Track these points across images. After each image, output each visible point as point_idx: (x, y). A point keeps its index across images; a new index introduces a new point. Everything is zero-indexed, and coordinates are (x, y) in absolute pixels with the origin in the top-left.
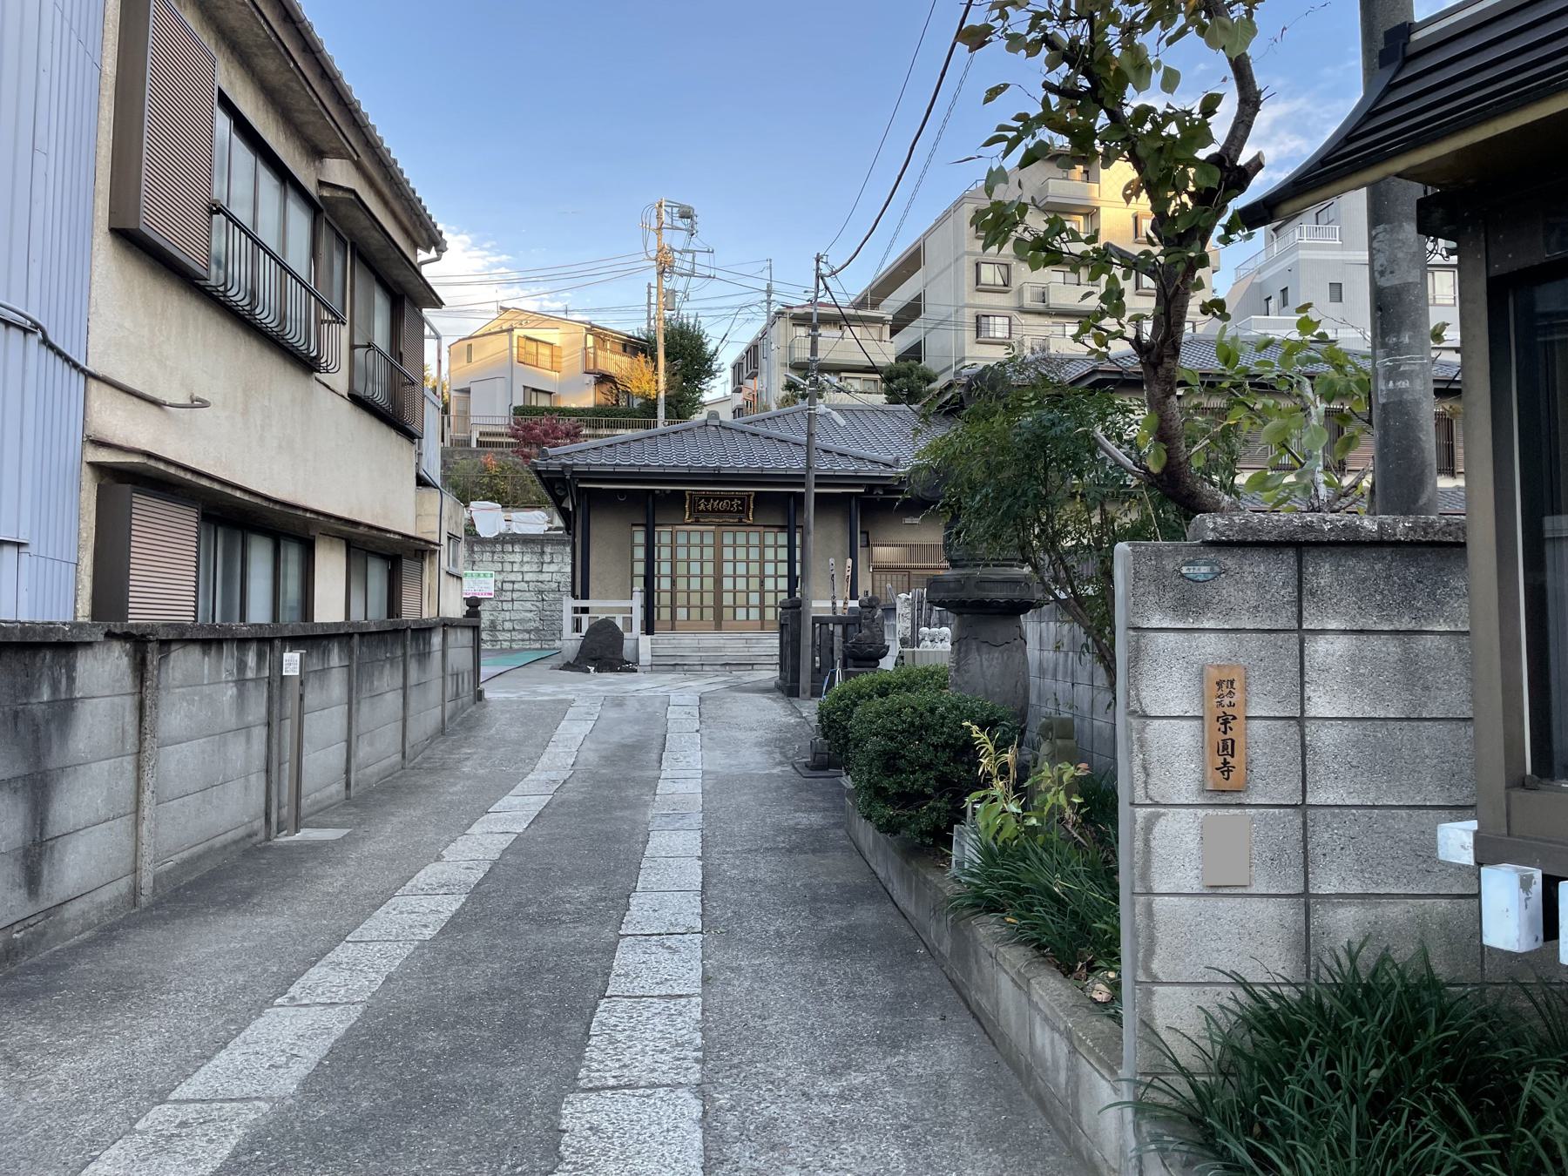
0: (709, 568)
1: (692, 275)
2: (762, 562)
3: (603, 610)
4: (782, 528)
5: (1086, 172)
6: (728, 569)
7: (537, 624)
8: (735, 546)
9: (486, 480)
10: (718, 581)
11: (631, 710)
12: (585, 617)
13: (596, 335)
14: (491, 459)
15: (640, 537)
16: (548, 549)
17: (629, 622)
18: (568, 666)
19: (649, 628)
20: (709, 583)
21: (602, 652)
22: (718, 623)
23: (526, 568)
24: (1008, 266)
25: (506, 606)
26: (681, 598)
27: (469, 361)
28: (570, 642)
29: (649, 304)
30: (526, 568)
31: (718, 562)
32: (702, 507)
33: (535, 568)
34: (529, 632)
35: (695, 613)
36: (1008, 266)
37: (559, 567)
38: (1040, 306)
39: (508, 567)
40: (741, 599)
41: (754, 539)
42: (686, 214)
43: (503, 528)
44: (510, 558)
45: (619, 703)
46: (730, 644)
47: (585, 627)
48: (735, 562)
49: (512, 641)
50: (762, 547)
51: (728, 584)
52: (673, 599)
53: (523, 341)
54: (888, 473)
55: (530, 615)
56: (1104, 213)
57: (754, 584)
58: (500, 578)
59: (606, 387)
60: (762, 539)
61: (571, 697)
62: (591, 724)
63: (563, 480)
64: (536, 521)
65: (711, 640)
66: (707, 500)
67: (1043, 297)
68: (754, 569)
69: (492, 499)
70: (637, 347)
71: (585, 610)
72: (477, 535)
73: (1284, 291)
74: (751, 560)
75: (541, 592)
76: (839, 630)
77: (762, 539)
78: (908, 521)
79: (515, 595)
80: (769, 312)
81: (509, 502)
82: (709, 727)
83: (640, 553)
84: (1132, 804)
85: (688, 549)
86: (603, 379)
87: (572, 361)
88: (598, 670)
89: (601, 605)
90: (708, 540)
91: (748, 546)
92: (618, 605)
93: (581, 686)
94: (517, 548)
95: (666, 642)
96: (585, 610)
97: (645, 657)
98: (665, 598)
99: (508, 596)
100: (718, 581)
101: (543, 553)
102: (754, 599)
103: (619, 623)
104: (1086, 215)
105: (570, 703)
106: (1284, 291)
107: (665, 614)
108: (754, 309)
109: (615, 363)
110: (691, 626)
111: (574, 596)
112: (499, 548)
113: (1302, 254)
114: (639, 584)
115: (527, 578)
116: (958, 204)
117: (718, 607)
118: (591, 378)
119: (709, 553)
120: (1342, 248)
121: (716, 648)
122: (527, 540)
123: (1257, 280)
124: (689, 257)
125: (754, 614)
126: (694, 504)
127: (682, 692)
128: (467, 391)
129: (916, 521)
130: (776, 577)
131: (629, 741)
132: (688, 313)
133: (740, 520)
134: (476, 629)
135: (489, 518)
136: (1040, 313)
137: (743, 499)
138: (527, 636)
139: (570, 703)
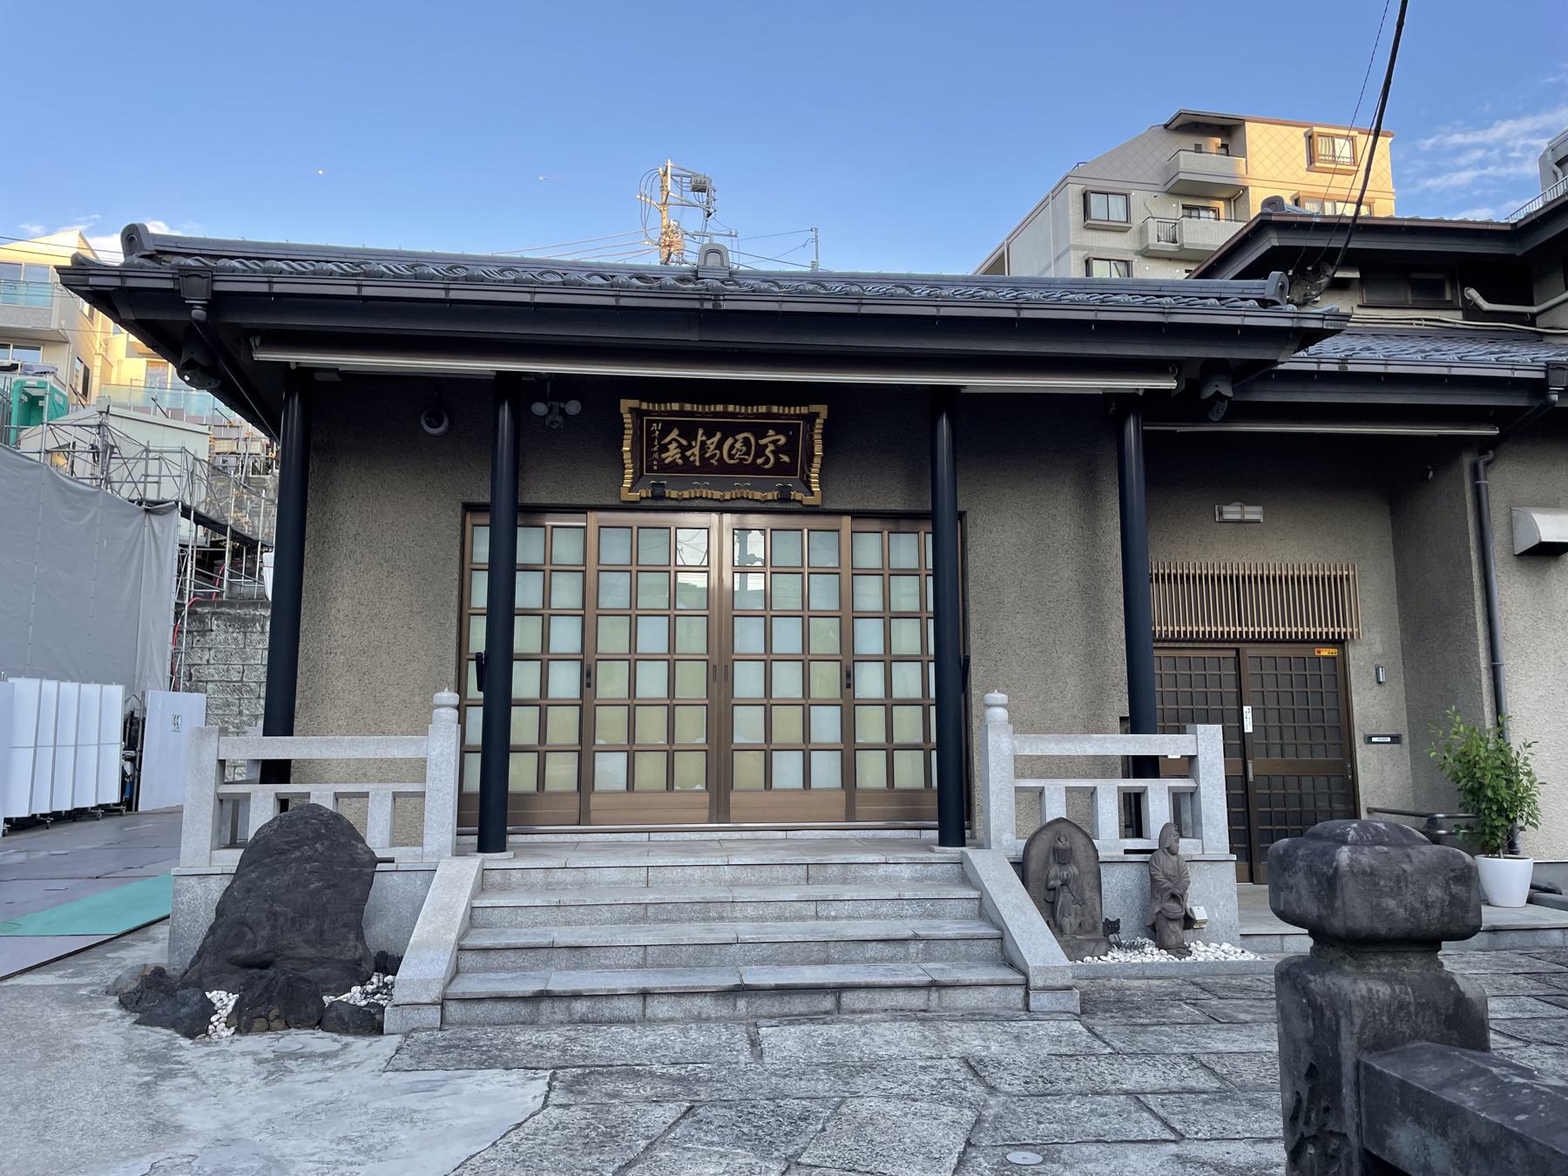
2: (848, 616)
4: (896, 520)
5: (1224, 146)
10: (720, 673)
17: (409, 808)
20: (692, 681)
22: (720, 799)
26: (610, 724)
32: (672, 454)
35: (651, 770)
40: (787, 724)
41: (824, 552)
48: (768, 660)
51: (748, 681)
52: (586, 727)
57: (826, 679)
66: (688, 432)
78: (1232, 512)
84: (584, 572)
92: (393, 761)
102: (826, 724)
104: (1228, 200)
116: (1063, 183)
125: (826, 770)
126: (648, 447)
129: (1254, 513)
130: (889, 659)
133: (785, 498)
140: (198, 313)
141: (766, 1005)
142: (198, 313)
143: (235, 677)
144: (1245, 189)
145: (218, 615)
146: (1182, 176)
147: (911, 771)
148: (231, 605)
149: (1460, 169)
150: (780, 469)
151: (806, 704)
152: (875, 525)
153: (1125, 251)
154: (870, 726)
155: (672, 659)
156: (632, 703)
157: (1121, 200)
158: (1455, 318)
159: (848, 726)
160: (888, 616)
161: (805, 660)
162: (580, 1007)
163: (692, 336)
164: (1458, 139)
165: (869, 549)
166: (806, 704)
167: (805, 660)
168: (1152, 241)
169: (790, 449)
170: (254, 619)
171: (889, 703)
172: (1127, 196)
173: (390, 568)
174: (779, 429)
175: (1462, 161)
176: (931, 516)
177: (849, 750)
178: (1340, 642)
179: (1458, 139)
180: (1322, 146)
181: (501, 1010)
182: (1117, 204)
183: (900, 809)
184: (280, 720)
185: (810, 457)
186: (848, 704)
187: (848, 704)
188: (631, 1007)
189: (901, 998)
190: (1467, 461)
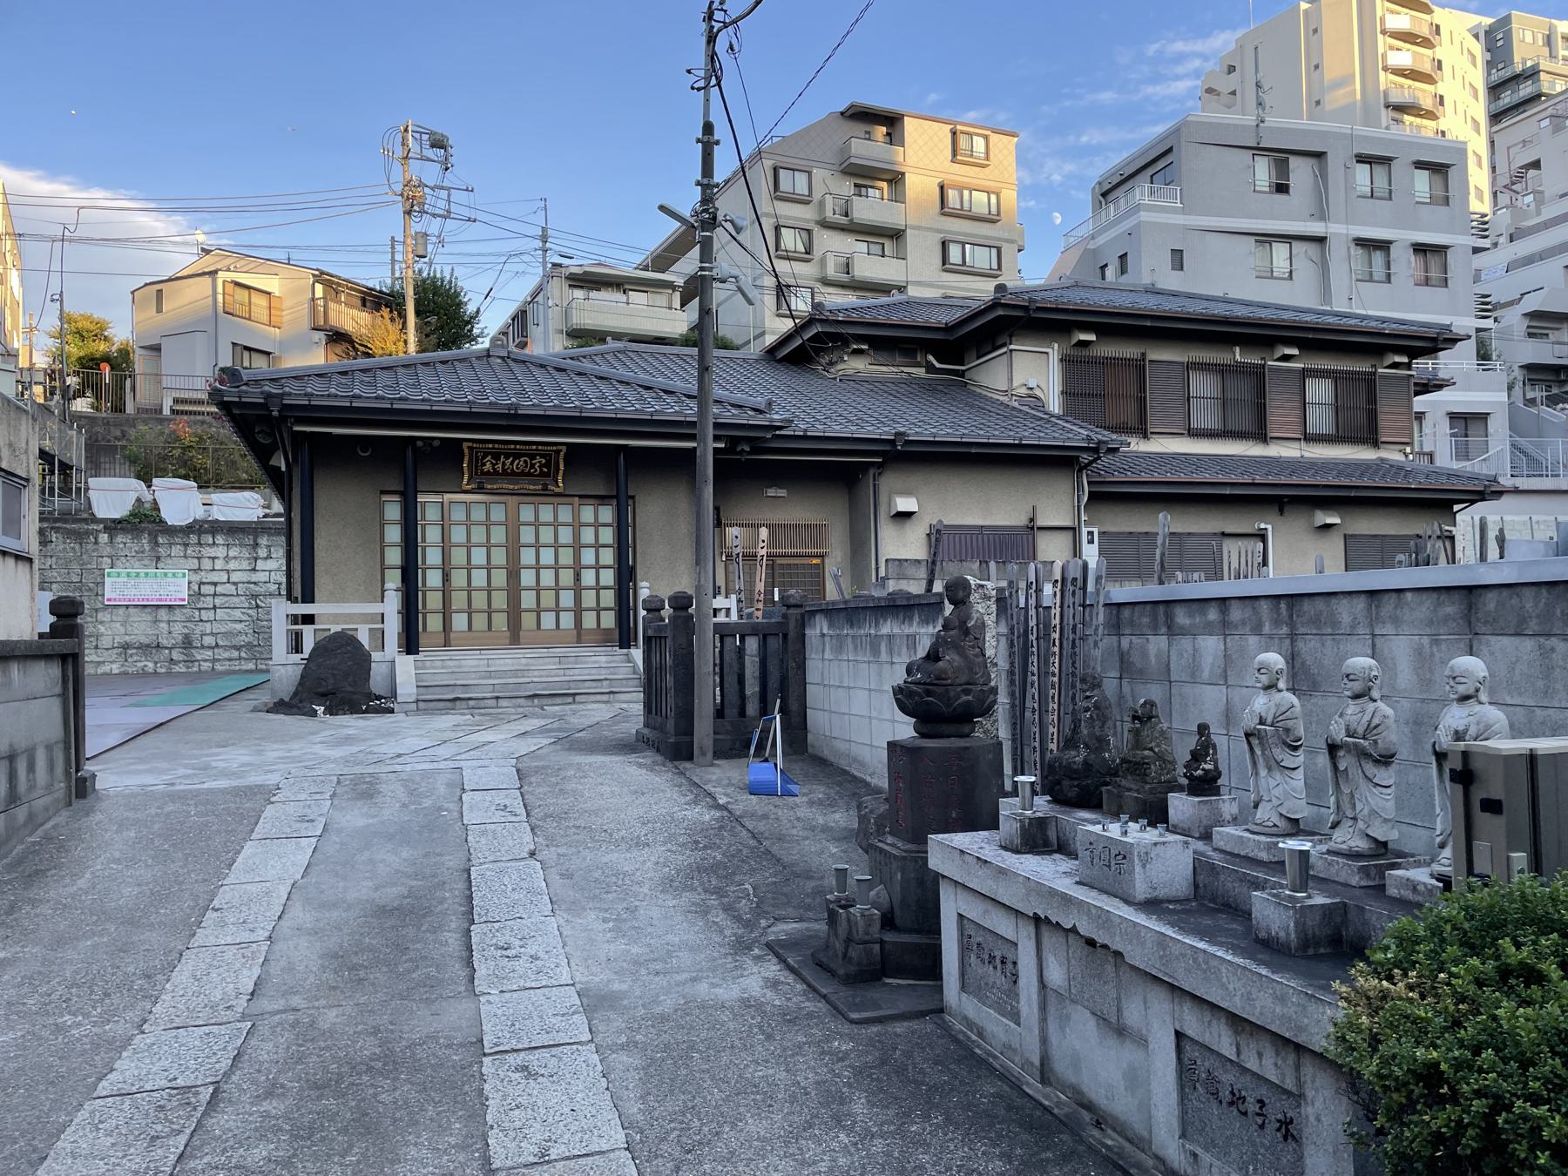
0: (499, 557)
1: (447, 216)
2: (577, 546)
3: (336, 618)
4: (602, 499)
5: (888, 134)
6: (527, 557)
7: (249, 639)
8: (537, 524)
9: (177, 453)
10: (514, 574)
11: (391, 806)
12: (308, 630)
13: (328, 284)
14: (185, 430)
15: (393, 511)
16: (263, 541)
17: (379, 637)
18: (281, 707)
19: (410, 644)
20: (500, 578)
21: (337, 682)
22: (515, 636)
23: (232, 565)
24: (809, 232)
25: (205, 615)
26: (459, 600)
27: (159, 310)
28: (286, 667)
29: (393, 261)
30: (232, 565)
31: (513, 548)
32: (488, 467)
33: (245, 565)
34: (238, 648)
35: (480, 621)
36: (809, 232)
37: (273, 566)
38: (844, 278)
39: (207, 564)
40: (548, 599)
41: (565, 514)
42: (439, 143)
43: (199, 513)
44: (212, 552)
45: (364, 789)
46: (536, 665)
47: (308, 644)
49: (214, 660)
50: (577, 526)
51: (527, 578)
52: (446, 601)
53: (230, 287)
54: (760, 420)
55: (239, 627)
56: (910, 179)
57: (567, 577)
58: (196, 578)
59: (339, 349)
60: (576, 515)
61: (273, 779)
62: (308, 845)
63: (268, 418)
64: (247, 505)
65: (507, 660)
66: (496, 457)
67: (847, 268)
68: (566, 557)
69: (186, 477)
70: (379, 301)
71: (309, 619)
72: (162, 521)
73: (1123, 257)
74: (564, 540)
75: (255, 596)
76: (752, 644)
77: (576, 515)
78: (771, 492)
79: (218, 601)
80: (544, 263)
81: (206, 481)
82: (551, 841)
83: (394, 534)
85: (464, 527)
86: (337, 337)
87: (295, 315)
88: (330, 711)
89: (335, 611)
90: (498, 513)
91: (556, 525)
92: (360, 609)
93: (297, 748)
94: (220, 540)
95: (437, 664)
96: (309, 619)
97: (407, 687)
98: (434, 601)
99: (209, 602)
100: (514, 574)
101: (256, 545)
102: (567, 599)
103: (363, 637)
104: (890, 181)
105: (266, 794)
106: (1123, 257)
107: (434, 623)
108: (526, 258)
109: (352, 319)
110: (473, 640)
111: (290, 597)
112: (193, 539)
113: (1144, 216)
114: (394, 580)
115: (235, 577)
117: (514, 612)
118: (320, 337)
119: (499, 535)
120: (1183, 211)
121: (516, 673)
122: (234, 530)
123: (1091, 246)
124: (444, 194)
125: (567, 620)
126: (476, 464)
127: (488, 754)
128: (157, 349)
129: (782, 493)
130: (598, 567)
131: (391, 894)
132: (442, 265)
133: (545, 488)
134: (71, 662)
135: (179, 501)
136: (843, 286)
137: (550, 457)
138: (235, 654)
139: (266, 794)
140: (275, 413)
141: (545, 701)
142: (275, 413)
143: (76, 579)
144: (903, 174)
145: (57, 530)
146: (853, 160)
147: (609, 620)
148: (66, 521)
149: (1178, 78)
150: (542, 474)
151: (557, 589)
152: (592, 501)
153: (808, 221)
154: (589, 599)
155: (489, 568)
156: (469, 589)
157: (804, 176)
158: (920, 372)
159: (578, 599)
160: (597, 546)
161: (556, 568)
162: (472, 703)
163: (504, 423)
164: (1180, 46)
165: (587, 513)
166: (557, 589)
167: (556, 568)
168: (829, 213)
169: (548, 465)
170: (88, 533)
171: (598, 588)
172: (810, 173)
173: (354, 522)
174: (542, 456)
175: (1180, 70)
176: (616, 497)
177: (578, 611)
178: (822, 556)
179: (1180, 46)
180: (963, 142)
181: (442, 704)
182: (801, 179)
183: (603, 638)
184: (308, 597)
185: (558, 470)
186: (578, 589)
187: (578, 589)
188: (492, 703)
189: (599, 697)
190: (871, 472)
